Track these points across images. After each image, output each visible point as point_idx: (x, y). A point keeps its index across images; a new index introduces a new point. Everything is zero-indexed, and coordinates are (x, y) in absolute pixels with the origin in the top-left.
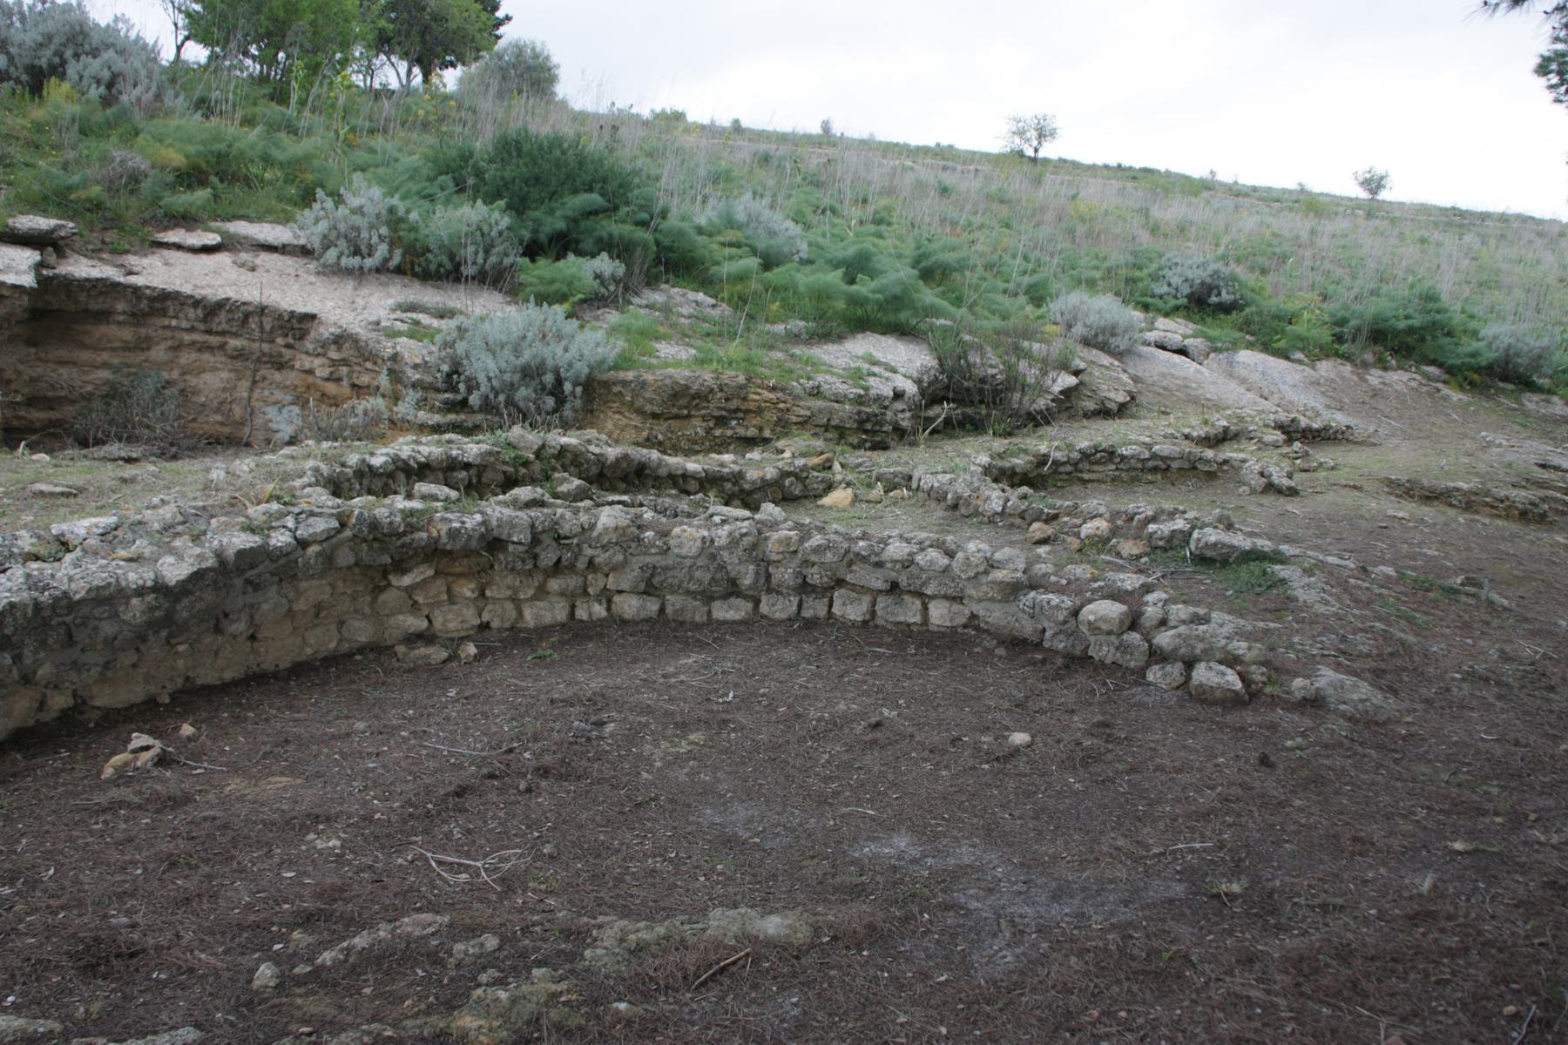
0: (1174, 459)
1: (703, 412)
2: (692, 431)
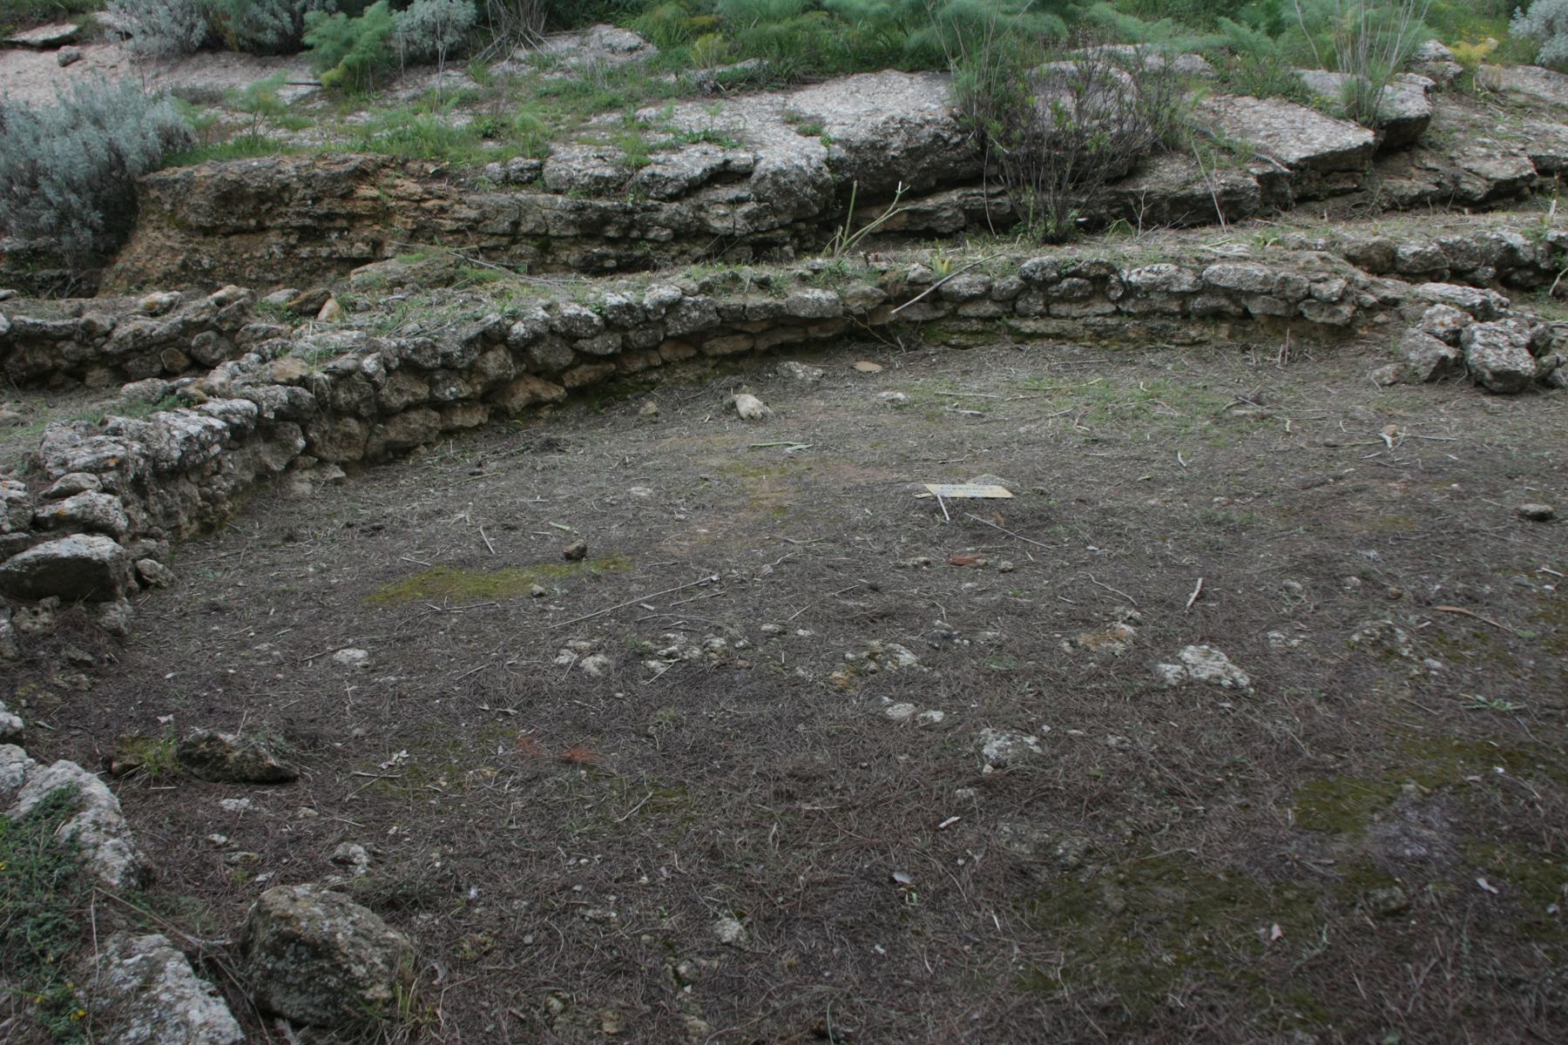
0: (1250, 295)
1: (280, 221)
2: (264, 251)
